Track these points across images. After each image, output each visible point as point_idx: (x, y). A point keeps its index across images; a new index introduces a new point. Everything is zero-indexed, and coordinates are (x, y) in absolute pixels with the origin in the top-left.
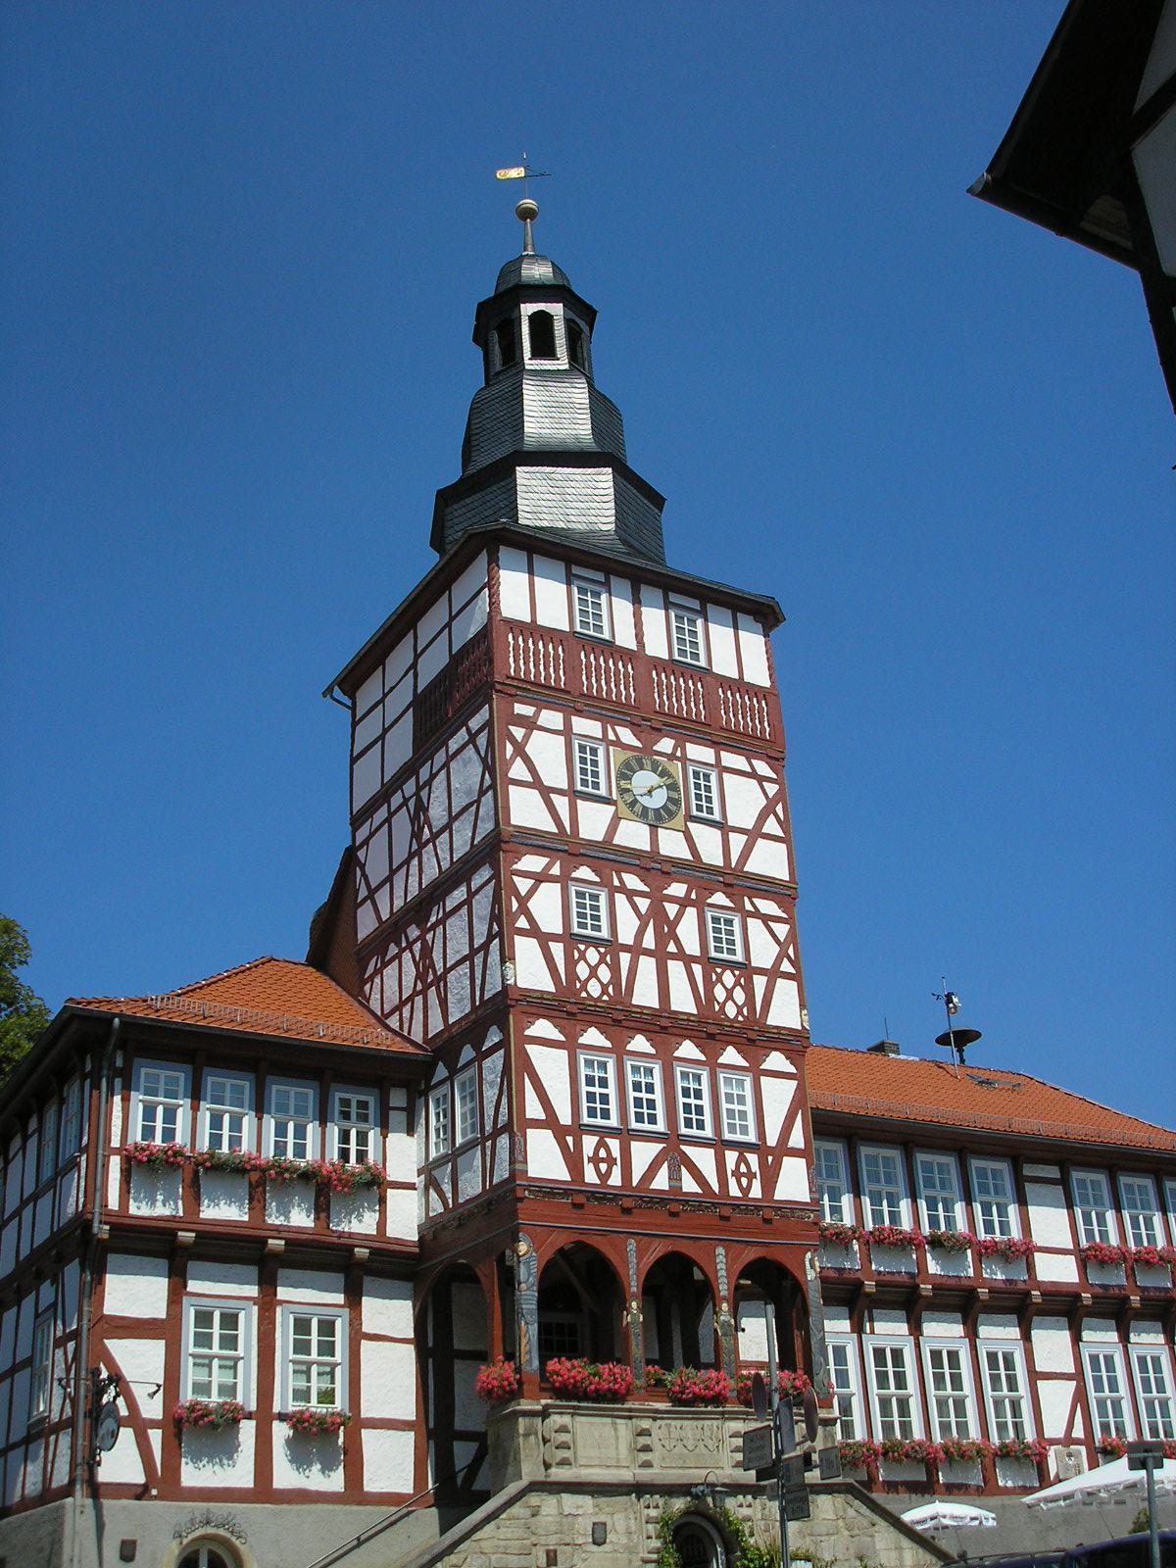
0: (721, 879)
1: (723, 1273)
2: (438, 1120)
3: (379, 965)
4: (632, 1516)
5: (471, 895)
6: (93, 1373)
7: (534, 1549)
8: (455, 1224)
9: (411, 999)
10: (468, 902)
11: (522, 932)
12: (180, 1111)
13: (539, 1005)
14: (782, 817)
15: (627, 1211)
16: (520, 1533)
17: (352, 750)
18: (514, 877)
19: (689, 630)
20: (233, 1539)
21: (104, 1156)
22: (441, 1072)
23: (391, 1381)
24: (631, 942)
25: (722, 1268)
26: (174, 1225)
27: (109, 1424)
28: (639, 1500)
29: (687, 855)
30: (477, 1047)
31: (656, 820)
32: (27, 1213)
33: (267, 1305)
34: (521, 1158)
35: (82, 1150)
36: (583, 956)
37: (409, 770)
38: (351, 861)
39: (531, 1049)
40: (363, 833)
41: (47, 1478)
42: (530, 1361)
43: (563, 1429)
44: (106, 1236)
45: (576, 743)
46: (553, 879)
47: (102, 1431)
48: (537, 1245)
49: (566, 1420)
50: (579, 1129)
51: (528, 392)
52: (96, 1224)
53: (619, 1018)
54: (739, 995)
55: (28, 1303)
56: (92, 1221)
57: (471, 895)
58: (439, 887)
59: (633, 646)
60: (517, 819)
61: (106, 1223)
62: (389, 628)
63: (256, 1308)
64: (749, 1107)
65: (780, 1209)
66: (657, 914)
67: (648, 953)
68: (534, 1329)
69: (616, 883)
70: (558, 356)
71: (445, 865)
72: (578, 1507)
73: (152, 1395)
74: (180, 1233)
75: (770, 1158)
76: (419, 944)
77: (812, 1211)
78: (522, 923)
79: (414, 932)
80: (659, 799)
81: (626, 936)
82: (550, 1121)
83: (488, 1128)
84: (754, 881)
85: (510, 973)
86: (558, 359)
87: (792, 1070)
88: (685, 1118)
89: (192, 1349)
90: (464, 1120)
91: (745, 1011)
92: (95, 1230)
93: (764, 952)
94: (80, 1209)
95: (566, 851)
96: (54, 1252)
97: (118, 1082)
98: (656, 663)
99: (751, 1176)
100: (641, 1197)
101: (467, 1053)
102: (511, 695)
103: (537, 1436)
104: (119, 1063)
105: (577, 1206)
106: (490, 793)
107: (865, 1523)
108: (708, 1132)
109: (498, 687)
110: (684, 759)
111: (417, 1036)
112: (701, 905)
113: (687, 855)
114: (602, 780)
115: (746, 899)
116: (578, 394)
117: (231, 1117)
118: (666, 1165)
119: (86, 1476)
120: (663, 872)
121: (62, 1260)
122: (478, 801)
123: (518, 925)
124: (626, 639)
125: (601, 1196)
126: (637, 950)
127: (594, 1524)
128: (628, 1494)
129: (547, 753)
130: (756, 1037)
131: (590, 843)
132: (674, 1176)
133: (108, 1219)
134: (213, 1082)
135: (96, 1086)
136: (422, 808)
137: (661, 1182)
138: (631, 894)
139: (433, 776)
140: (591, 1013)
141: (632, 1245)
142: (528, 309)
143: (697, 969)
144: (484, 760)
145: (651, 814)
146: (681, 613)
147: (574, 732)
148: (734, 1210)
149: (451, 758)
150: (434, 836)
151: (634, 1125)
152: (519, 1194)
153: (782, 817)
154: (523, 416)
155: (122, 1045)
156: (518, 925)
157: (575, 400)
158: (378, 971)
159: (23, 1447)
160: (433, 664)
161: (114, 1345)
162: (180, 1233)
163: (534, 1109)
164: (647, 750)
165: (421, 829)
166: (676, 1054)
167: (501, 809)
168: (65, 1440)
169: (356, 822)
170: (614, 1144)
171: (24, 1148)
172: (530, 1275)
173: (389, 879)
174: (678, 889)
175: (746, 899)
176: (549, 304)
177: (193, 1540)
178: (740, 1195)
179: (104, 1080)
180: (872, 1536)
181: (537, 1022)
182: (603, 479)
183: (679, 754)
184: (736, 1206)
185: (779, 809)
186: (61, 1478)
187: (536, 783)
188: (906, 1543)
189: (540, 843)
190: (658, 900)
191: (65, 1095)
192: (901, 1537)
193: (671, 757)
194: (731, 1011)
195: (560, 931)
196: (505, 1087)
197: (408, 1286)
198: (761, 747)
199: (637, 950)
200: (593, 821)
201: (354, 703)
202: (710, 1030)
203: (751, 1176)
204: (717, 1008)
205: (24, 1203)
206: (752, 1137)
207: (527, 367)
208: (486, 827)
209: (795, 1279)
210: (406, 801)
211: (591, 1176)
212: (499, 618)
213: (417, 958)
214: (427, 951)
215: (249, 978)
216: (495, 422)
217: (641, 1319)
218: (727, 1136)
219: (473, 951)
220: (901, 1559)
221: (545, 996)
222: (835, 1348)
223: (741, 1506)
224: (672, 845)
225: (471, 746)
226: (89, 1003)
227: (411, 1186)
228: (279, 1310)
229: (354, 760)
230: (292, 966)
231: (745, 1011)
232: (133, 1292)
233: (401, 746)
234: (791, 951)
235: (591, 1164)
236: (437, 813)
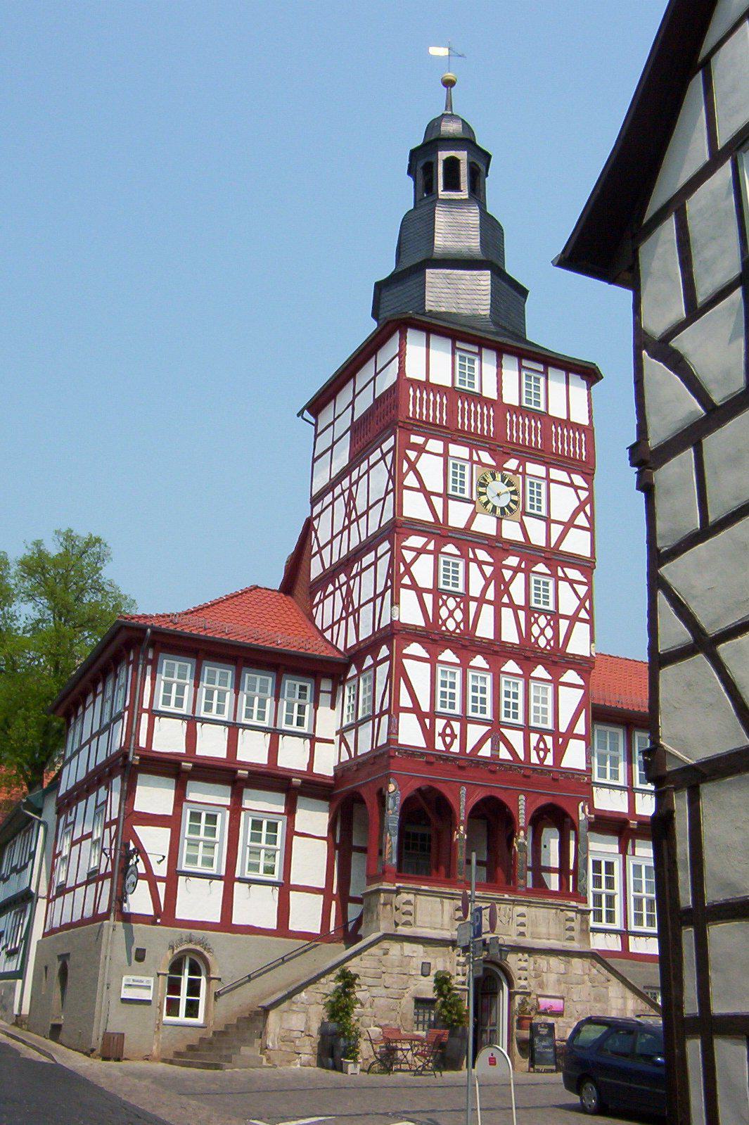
0: (543, 555)
1: (523, 812)
2: (350, 701)
3: (322, 598)
4: (448, 961)
5: (377, 559)
6: (125, 846)
7: (383, 975)
8: (355, 768)
9: (339, 622)
10: (374, 563)
11: (406, 586)
12: (187, 687)
13: (412, 634)
14: (589, 514)
15: (461, 768)
16: (375, 964)
17: (314, 454)
18: (403, 550)
19: (535, 386)
20: (205, 953)
21: (138, 713)
22: (353, 671)
23: (311, 862)
24: (478, 595)
25: (522, 810)
26: (180, 758)
27: (132, 878)
28: (453, 951)
29: (521, 539)
30: (374, 658)
31: (501, 514)
32: (94, 742)
33: (236, 809)
34: (394, 731)
35: (126, 709)
36: (445, 603)
37: (346, 472)
38: (308, 527)
39: (406, 662)
40: (317, 509)
41: (96, 907)
42: (391, 859)
43: (408, 903)
44: (137, 763)
45: (451, 462)
46: (429, 552)
47: (128, 882)
48: (400, 786)
49: (411, 897)
50: (433, 715)
51: (439, 216)
52: (131, 755)
53: (466, 644)
54: (549, 633)
55: (92, 798)
56: (129, 753)
57: (377, 559)
58: (359, 551)
59: (495, 397)
60: (408, 512)
61: (137, 755)
62: (362, 350)
63: (228, 812)
64: (550, 706)
65: (564, 773)
66: (497, 577)
67: (489, 602)
68: (395, 839)
69: (471, 556)
70: (462, 189)
71: (327, 565)
72: (414, 952)
73: (159, 862)
74: (183, 764)
75: (561, 740)
76: (345, 586)
77: (586, 776)
78: (406, 580)
79: (343, 578)
80: (504, 501)
81: (475, 591)
82: (416, 709)
83: (377, 711)
84: (565, 557)
85: (396, 612)
86: (461, 191)
87: (582, 683)
88: (505, 711)
89: (187, 835)
90: (364, 703)
91: (552, 643)
92: (131, 759)
93: (568, 604)
94: (123, 745)
95: (438, 534)
96: (107, 769)
97: (149, 668)
98: (510, 408)
99: (546, 750)
100: (472, 760)
101: (369, 661)
102: (408, 430)
103: (391, 905)
104: (150, 656)
105: (428, 763)
106: (392, 494)
107: (603, 979)
108: (520, 721)
109: (401, 424)
110: (524, 474)
111: (341, 646)
112: (527, 572)
113: (521, 539)
114: (467, 487)
115: (559, 568)
116: (472, 216)
117: (219, 693)
118: (490, 740)
119: (118, 908)
120: (504, 549)
121: (111, 775)
122: (384, 499)
123: (403, 582)
124: (490, 392)
125: (446, 758)
126: (481, 600)
127: (423, 963)
128: (447, 946)
129: (430, 469)
130: (558, 660)
131: (455, 530)
132: (495, 748)
133: (138, 752)
134: (208, 670)
135: (135, 670)
136: (352, 498)
137: (486, 751)
138: (480, 564)
139: (360, 478)
140: (448, 640)
141: (463, 791)
142: (443, 155)
143: (522, 614)
144: (389, 472)
145: (498, 511)
146: (529, 373)
147: (451, 454)
148: (533, 771)
149: (370, 467)
150: (359, 517)
151: (470, 713)
152: (392, 754)
153: (589, 514)
154: (434, 232)
155: (153, 644)
156: (403, 582)
157: (470, 222)
158: (322, 601)
159: (84, 887)
160: (364, 403)
161: (139, 829)
162: (183, 764)
163: (405, 701)
164: (500, 467)
165: (351, 512)
166: (502, 669)
167: (398, 505)
168: (107, 883)
169: (315, 500)
170: (456, 726)
171: (94, 702)
172: (395, 805)
173: (330, 542)
174: (513, 561)
175: (559, 568)
176: (457, 152)
177: (180, 952)
178: (538, 762)
179: (141, 666)
180: (607, 988)
181: (412, 645)
182: (484, 279)
183: (521, 470)
184: (534, 769)
185: (588, 509)
186: (103, 908)
187: (422, 489)
188: (629, 994)
189: (422, 529)
190: (498, 567)
191: (118, 672)
192: (627, 990)
193: (515, 472)
194: (542, 642)
195: (431, 587)
196: (388, 685)
197: (326, 804)
198: (578, 466)
199: (481, 600)
200: (458, 516)
201: (317, 422)
202: (527, 655)
203: (546, 750)
204: (533, 640)
205: (92, 737)
206: (550, 726)
207: (440, 197)
208: (388, 516)
209: (572, 820)
210: (343, 492)
211: (439, 745)
212: (404, 378)
213: (344, 596)
214: (349, 592)
215: (240, 600)
216: (416, 236)
217: (466, 837)
218: (532, 724)
219: (376, 596)
220: (625, 1004)
221: (418, 629)
222: (594, 862)
223: (520, 960)
224: (511, 531)
225: (382, 461)
226: (133, 618)
227: (331, 742)
228: (243, 814)
229: (314, 460)
230: (270, 592)
231: (552, 643)
232: (154, 796)
233: (342, 457)
234: (587, 605)
235: (440, 738)
236: (361, 505)
